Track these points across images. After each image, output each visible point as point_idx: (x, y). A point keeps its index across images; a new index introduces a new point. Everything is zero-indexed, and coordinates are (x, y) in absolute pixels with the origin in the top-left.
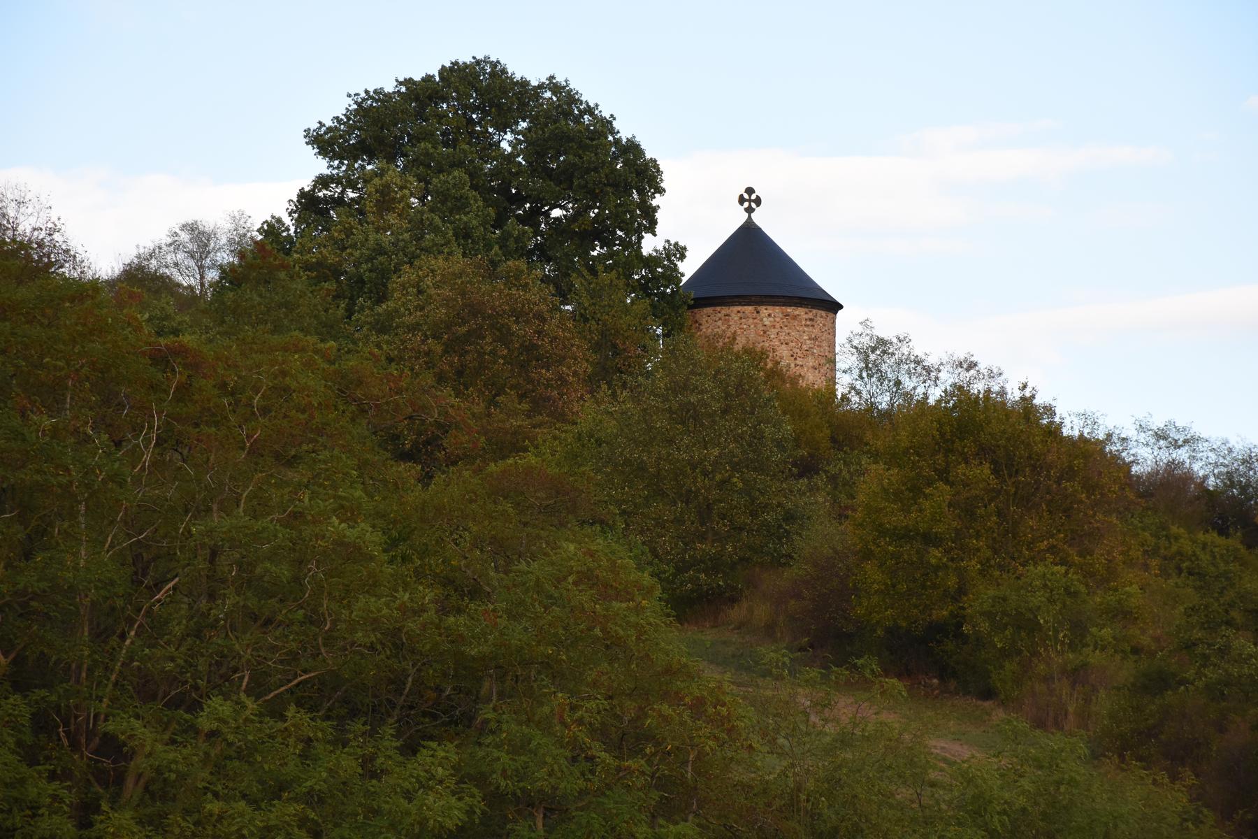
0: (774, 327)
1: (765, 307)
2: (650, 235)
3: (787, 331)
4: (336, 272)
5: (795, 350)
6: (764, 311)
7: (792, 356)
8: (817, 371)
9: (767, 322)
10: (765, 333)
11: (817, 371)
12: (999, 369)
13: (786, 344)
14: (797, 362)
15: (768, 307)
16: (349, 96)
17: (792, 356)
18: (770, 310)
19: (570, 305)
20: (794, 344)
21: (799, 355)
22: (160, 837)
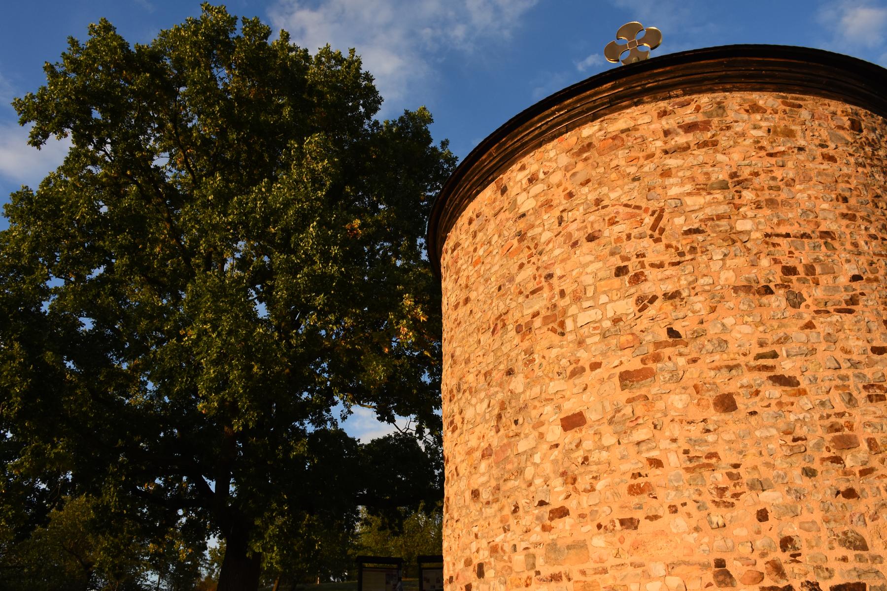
0: (548, 205)
1: (516, 167)
2: (310, 53)
3: (592, 197)
4: (826, 243)
5: (629, 248)
6: (515, 176)
7: (620, 271)
8: (778, 301)
9: (526, 203)
10: (521, 236)
11: (778, 301)
12: (106, 22)
13: (591, 238)
14: (647, 288)
15: (526, 160)
16: (202, 5)
17: (620, 271)
18: (532, 162)
19: (71, 177)
20: (621, 228)
21: (651, 258)
22: (658, 584)
